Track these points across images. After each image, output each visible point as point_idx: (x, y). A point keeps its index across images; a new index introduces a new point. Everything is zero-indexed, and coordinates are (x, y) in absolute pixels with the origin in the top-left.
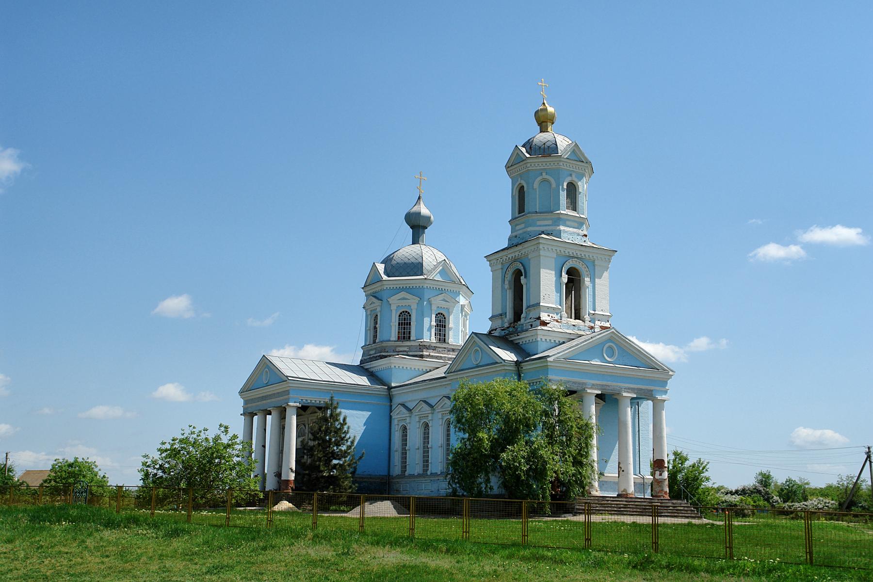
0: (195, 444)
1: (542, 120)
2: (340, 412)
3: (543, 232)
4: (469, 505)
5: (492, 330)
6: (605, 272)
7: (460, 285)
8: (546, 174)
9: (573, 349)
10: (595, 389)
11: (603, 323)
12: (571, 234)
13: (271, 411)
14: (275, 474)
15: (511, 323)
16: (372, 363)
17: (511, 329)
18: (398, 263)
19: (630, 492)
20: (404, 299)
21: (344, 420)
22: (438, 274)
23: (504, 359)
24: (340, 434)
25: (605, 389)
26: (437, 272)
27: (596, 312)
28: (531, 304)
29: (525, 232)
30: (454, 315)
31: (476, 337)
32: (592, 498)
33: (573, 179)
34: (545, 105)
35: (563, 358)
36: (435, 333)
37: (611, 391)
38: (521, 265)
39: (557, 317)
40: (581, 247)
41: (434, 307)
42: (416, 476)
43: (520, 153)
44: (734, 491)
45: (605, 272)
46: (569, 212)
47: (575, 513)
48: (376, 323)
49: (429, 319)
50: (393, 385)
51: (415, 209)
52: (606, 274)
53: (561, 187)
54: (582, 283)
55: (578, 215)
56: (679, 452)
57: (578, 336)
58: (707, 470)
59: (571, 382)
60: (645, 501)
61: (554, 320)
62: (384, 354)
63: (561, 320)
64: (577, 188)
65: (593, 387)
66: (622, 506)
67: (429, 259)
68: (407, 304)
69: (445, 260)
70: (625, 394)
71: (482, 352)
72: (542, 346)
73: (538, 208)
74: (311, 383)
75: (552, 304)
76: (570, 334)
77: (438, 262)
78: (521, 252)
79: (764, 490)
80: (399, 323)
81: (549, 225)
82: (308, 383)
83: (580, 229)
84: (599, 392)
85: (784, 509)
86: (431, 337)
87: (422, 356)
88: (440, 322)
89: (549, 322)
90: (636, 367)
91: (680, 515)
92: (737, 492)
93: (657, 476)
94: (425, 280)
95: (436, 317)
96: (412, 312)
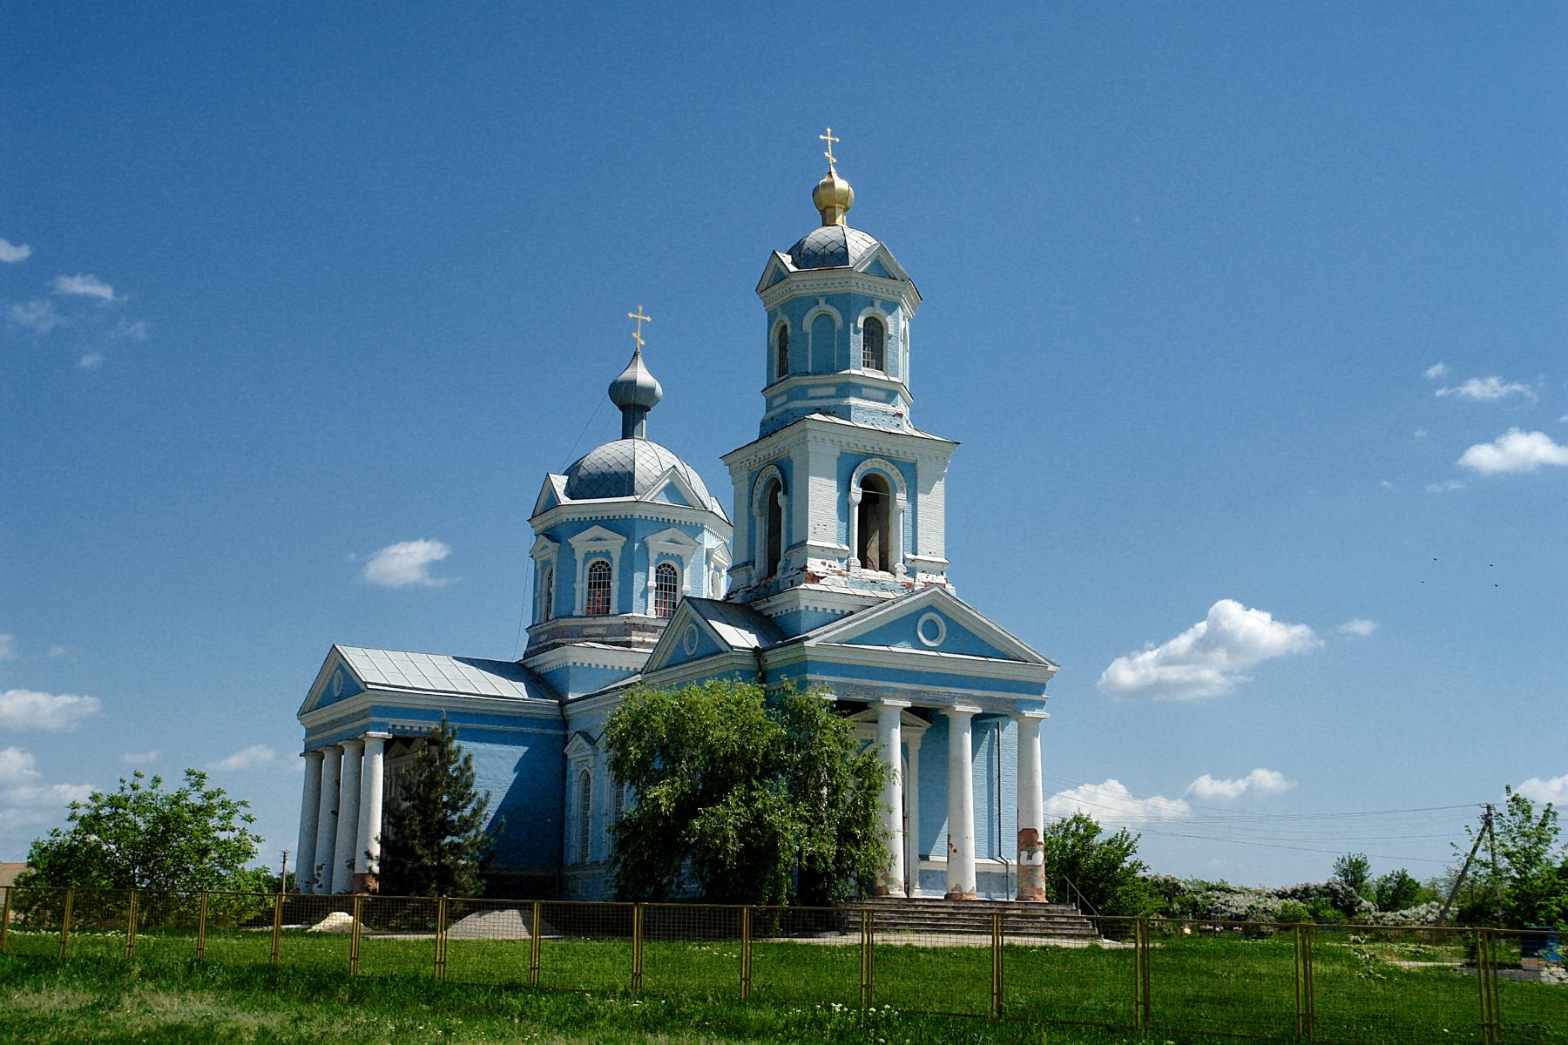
0: (140, 806)
3: (819, 409)
5: (732, 593)
7: (703, 513)
10: (900, 698)
11: (931, 576)
19: (968, 891)
21: (467, 760)
23: (731, 644)
24: (461, 787)
25: (921, 699)
26: (659, 489)
27: (918, 557)
28: (794, 542)
29: (787, 411)
33: (876, 312)
34: (831, 176)
39: (838, 566)
40: (889, 436)
41: (653, 556)
44: (1289, 892)
47: (846, 928)
48: (550, 584)
50: (571, 696)
52: (939, 487)
53: (852, 325)
55: (885, 378)
56: (1085, 816)
57: (878, 600)
58: (1134, 851)
59: (852, 685)
61: (834, 571)
65: (896, 693)
66: (942, 916)
67: (647, 465)
68: (604, 550)
70: (959, 708)
72: (804, 625)
74: (412, 696)
76: (864, 597)
77: (664, 470)
79: (1343, 888)
80: (590, 584)
82: (397, 694)
84: (909, 704)
85: (1366, 923)
86: (646, 608)
87: (629, 644)
89: (824, 575)
92: (1294, 894)
95: (657, 572)
96: (612, 563)
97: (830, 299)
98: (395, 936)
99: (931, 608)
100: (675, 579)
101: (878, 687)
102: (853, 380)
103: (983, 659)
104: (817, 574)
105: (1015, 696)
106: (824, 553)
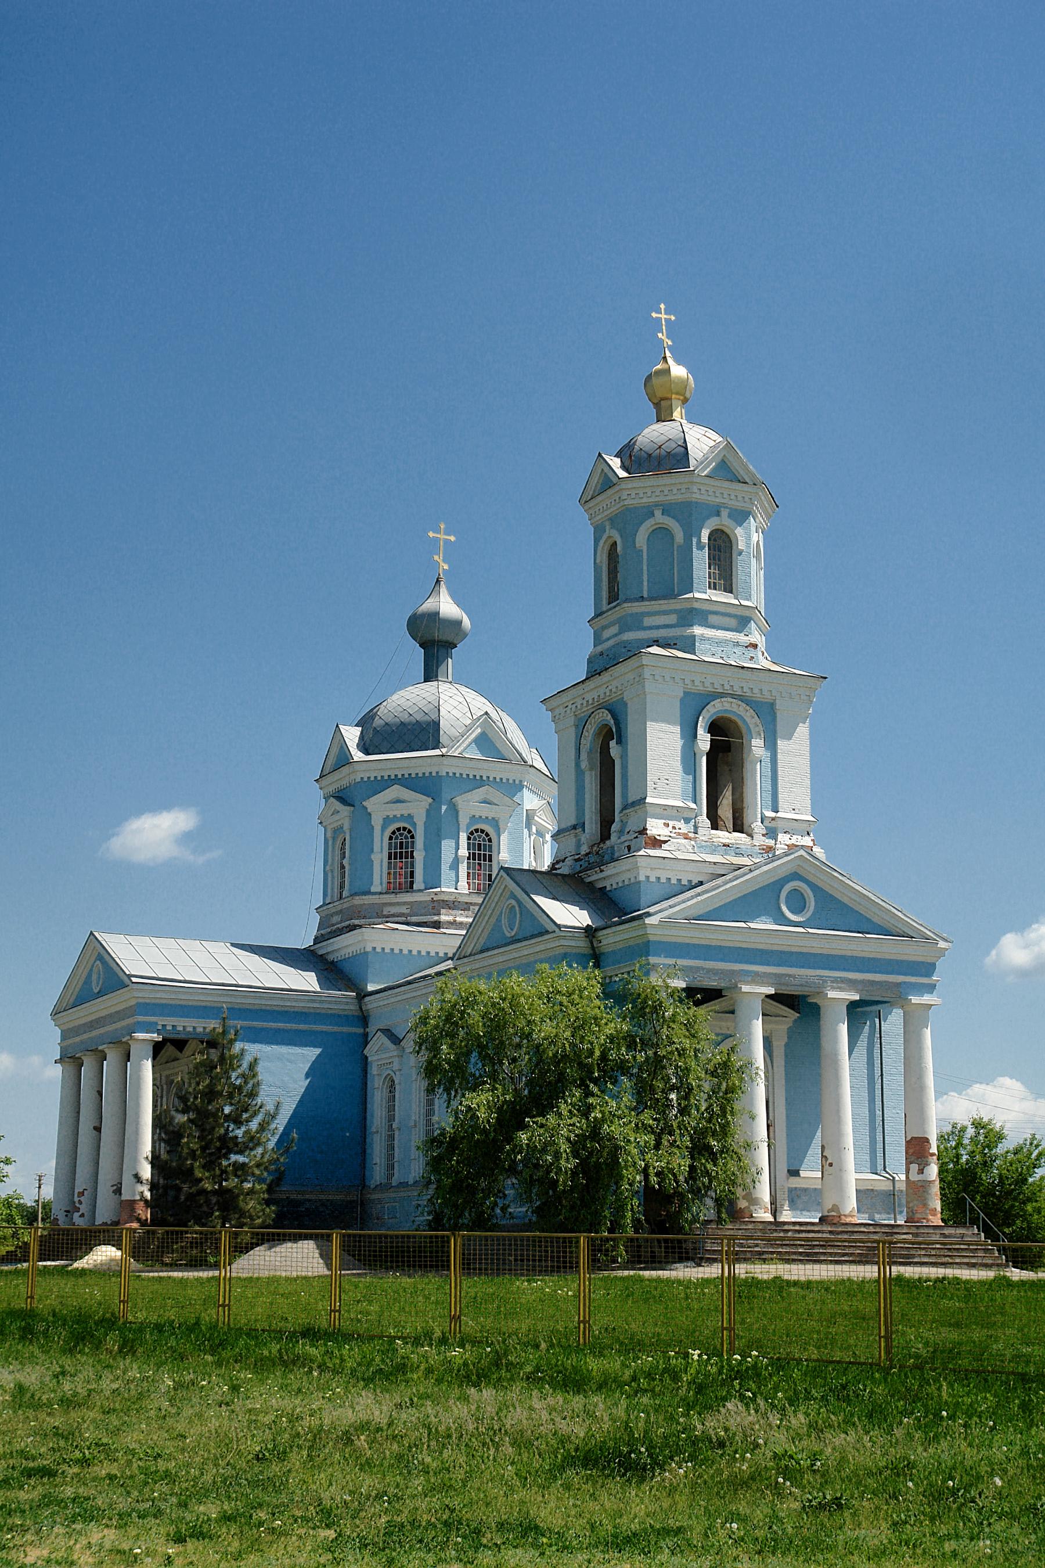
1: (660, 394)
2: (243, 1050)
3: (658, 641)
4: (232, 1244)
5: (558, 862)
6: (801, 725)
7: (522, 767)
9: (706, 896)
10: (762, 984)
11: (795, 837)
12: (719, 643)
13: (106, 1051)
14: (115, 1187)
15: (593, 846)
16: (331, 940)
17: (592, 859)
18: (387, 724)
19: (847, 1212)
20: (399, 801)
21: (252, 1066)
22: (473, 745)
27: (779, 815)
28: (630, 801)
30: (510, 833)
31: (508, 878)
32: (750, 1226)
35: (683, 916)
36: (468, 873)
37: (800, 988)
38: (610, 716)
39: (685, 828)
40: (741, 671)
41: (464, 820)
42: (411, 1186)
43: (606, 470)
45: (801, 725)
46: (716, 595)
47: (701, 1259)
49: (453, 843)
50: (371, 988)
51: (428, 606)
53: (695, 541)
54: (745, 751)
55: (736, 602)
60: (878, 1230)
61: (679, 834)
62: (356, 922)
63: (696, 833)
64: (734, 541)
65: (757, 978)
67: (454, 712)
68: (405, 813)
69: (486, 713)
70: (831, 994)
71: (521, 914)
73: (645, 588)
75: (675, 798)
76: (715, 863)
78: (610, 688)
83: (740, 632)
84: (771, 991)
86: (457, 881)
87: (437, 925)
88: (479, 850)
89: (666, 839)
90: (859, 932)
91: (957, 1260)
93: (914, 1177)
94: (441, 758)
95: (469, 838)
96: (415, 831)
97: (667, 510)
99: (795, 876)
100: (490, 847)
102: (696, 605)
104: (658, 838)
105: (900, 978)
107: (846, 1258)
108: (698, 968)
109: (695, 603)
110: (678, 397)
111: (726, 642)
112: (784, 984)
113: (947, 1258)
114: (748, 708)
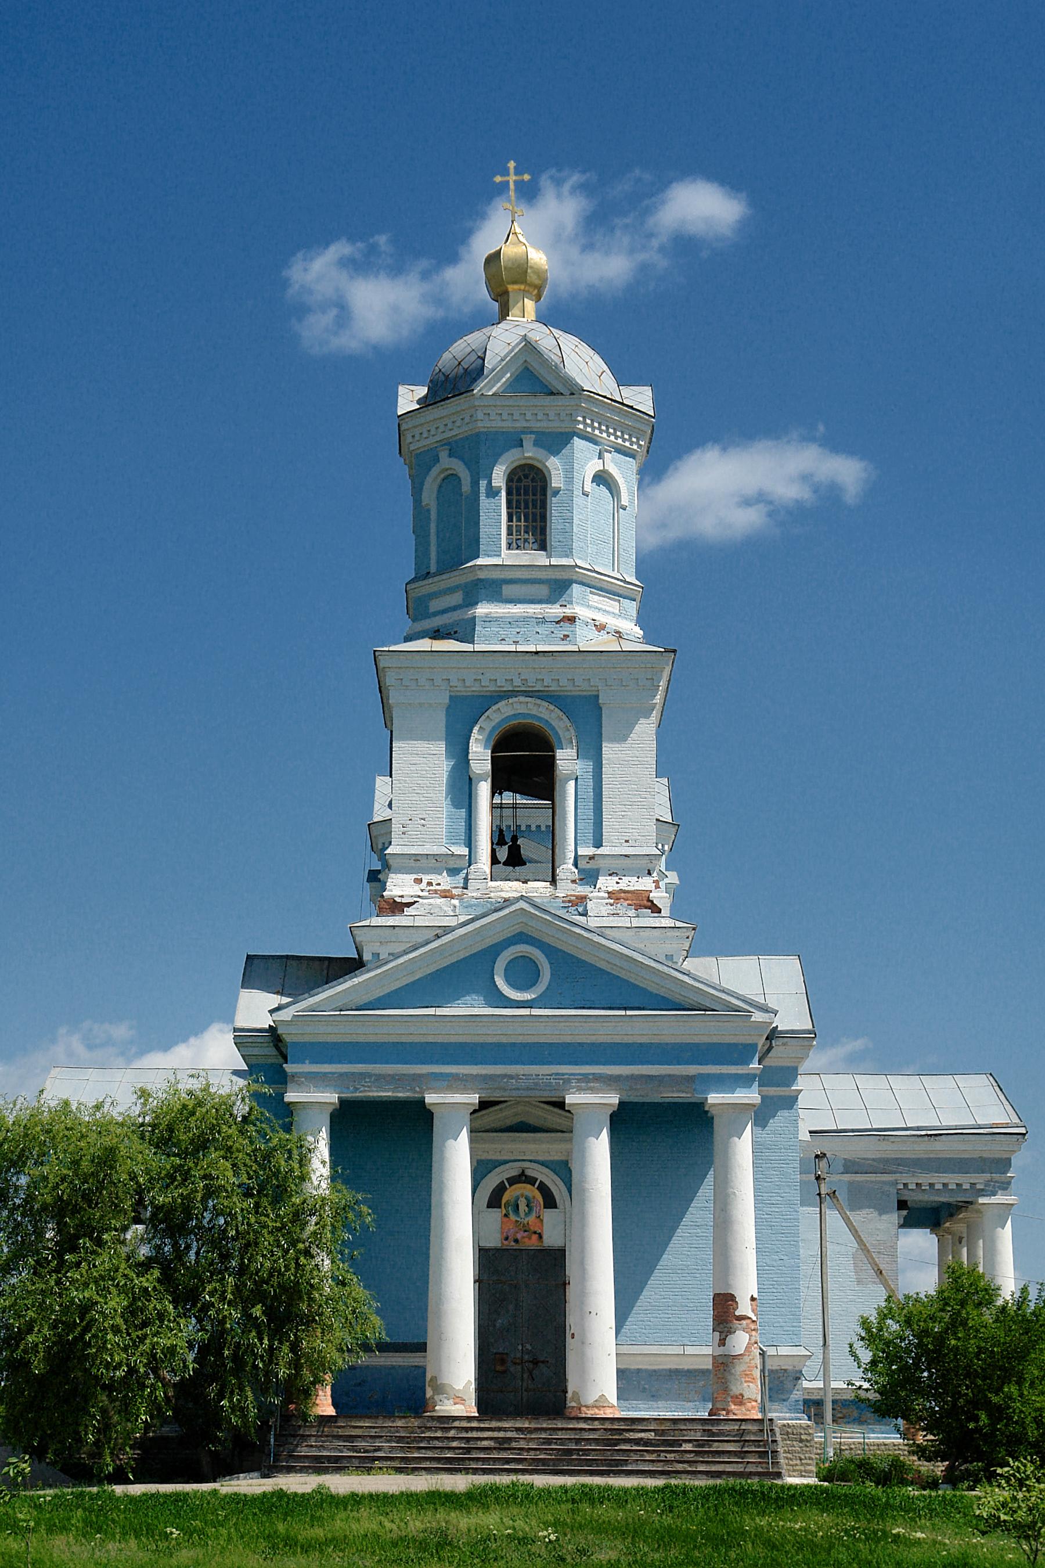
8: (450, 456)
10: (465, 1090)
11: (625, 879)
19: (590, 1401)
39: (445, 881)
40: (535, 657)
53: (483, 484)
61: (436, 892)
65: (587, 1082)
66: (485, 1443)
81: (454, 608)
90: (619, 1009)
97: (454, 448)
98: (89, 1489)
99: (521, 938)
101: (420, 1076)
102: (482, 575)
103: (622, 1013)
104: (398, 900)
105: (692, 1070)
106: (417, 864)
107: (512, 1466)
108: (361, 1074)
109: (478, 572)
110: (516, 287)
111: (525, 619)
112: (499, 1088)
113: (685, 1466)
114: (552, 707)
